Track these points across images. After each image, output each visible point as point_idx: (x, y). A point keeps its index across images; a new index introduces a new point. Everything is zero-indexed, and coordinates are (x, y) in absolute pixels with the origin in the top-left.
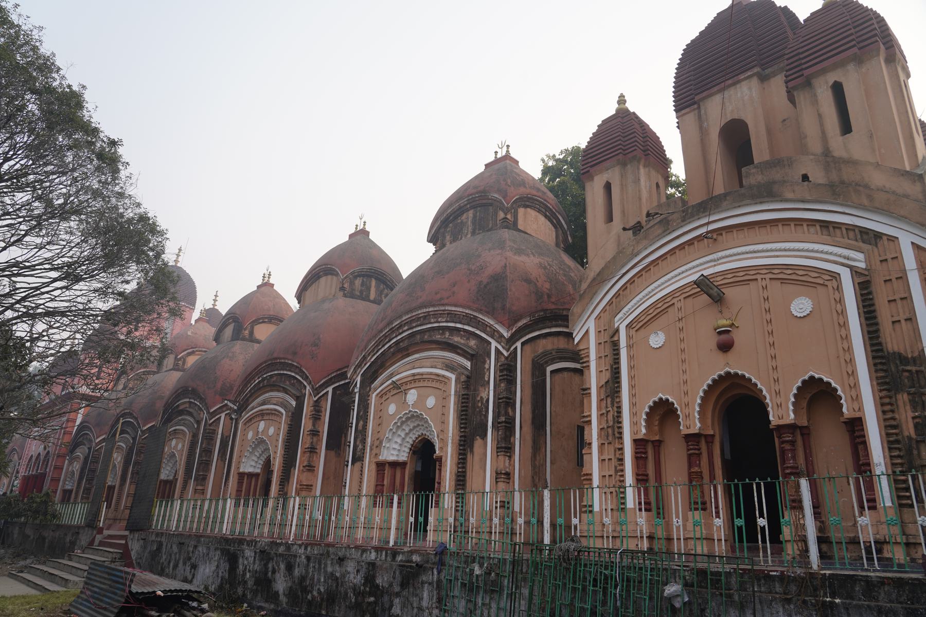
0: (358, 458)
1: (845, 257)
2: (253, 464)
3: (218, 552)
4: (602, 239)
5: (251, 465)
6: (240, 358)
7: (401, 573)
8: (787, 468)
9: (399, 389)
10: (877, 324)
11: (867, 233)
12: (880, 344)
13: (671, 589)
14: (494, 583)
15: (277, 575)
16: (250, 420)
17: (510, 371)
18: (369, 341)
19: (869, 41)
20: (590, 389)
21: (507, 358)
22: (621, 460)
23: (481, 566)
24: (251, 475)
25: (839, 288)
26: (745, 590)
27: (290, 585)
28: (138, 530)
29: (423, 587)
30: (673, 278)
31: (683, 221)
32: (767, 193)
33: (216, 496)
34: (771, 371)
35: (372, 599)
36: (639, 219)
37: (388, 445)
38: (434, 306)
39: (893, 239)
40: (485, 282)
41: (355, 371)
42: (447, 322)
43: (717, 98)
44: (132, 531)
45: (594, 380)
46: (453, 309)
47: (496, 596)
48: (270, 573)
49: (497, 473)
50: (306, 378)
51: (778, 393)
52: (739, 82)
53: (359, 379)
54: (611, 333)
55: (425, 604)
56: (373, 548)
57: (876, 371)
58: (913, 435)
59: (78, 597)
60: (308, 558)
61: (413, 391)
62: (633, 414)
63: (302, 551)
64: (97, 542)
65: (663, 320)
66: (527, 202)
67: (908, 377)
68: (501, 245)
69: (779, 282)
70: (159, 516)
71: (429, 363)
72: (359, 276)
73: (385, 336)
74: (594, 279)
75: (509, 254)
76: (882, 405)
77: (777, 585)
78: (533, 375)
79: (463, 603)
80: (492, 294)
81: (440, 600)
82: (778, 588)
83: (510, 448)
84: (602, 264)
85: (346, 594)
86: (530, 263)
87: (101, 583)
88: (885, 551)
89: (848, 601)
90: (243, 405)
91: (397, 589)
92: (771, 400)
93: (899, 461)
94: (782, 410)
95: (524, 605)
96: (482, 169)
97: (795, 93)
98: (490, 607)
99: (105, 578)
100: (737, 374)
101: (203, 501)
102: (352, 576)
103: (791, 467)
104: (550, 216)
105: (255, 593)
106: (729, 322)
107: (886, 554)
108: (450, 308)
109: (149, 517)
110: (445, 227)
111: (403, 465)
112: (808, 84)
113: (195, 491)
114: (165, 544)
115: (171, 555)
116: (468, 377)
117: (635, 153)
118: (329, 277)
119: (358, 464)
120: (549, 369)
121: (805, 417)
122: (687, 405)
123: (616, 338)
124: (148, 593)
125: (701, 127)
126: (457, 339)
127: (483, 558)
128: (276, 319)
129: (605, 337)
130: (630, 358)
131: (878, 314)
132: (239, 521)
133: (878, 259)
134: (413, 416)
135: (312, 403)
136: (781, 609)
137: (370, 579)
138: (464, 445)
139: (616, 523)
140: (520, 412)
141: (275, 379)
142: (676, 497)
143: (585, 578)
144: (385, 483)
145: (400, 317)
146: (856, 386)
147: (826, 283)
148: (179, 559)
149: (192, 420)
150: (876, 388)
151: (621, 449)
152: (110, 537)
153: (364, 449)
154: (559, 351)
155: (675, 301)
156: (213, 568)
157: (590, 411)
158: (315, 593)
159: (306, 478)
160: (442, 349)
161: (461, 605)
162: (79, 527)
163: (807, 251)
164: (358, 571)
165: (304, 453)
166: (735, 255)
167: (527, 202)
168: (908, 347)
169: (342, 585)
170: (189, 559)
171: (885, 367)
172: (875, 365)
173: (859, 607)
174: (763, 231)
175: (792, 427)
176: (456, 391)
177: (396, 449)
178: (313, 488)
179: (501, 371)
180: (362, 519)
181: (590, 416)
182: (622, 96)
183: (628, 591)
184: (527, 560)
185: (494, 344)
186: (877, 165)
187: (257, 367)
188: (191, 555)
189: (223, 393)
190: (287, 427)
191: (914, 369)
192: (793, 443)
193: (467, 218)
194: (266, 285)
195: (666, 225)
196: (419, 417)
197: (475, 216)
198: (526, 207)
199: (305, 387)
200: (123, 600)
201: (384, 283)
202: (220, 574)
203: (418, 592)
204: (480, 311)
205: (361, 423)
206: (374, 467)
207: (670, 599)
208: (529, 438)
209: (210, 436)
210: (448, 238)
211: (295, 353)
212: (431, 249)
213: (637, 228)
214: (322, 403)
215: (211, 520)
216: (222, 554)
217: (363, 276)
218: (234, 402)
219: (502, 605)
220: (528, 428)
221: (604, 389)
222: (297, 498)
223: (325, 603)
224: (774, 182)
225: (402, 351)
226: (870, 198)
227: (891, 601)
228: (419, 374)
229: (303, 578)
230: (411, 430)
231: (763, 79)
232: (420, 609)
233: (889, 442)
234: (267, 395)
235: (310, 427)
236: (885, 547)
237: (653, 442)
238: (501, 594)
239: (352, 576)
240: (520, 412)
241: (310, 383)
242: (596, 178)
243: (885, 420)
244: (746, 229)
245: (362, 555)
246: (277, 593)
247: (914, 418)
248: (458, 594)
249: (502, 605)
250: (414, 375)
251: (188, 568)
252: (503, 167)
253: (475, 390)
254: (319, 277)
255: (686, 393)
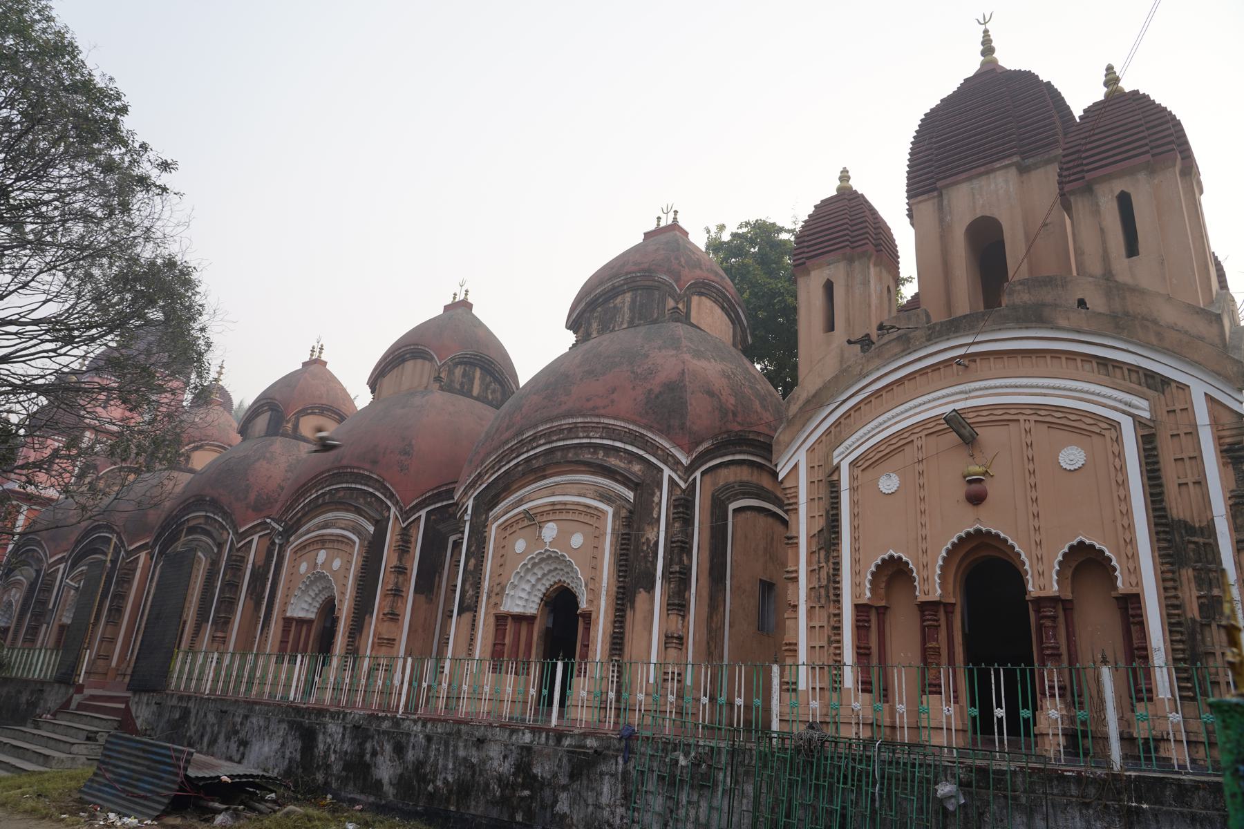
0: (469, 607)
1: (1126, 404)
2: (306, 606)
3: (284, 726)
4: (817, 354)
5: (303, 608)
6: (284, 461)
7: (570, 761)
8: (1048, 648)
9: (533, 520)
10: (1161, 485)
11: (1153, 377)
12: (1164, 509)
13: (945, 789)
14: (705, 776)
15: (380, 759)
16: (303, 547)
17: (687, 508)
18: (489, 454)
19: (1165, 148)
20: (797, 537)
21: (683, 491)
22: (838, 629)
23: (686, 755)
24: (301, 622)
25: (1118, 440)
26: (1034, 792)
27: (399, 771)
28: (153, 691)
29: (602, 779)
30: (911, 409)
31: (928, 340)
32: (1035, 316)
33: (245, 647)
34: (1032, 532)
35: (527, 793)
36: (867, 331)
37: (512, 593)
38: (584, 416)
39: (1183, 387)
40: (657, 390)
41: (465, 493)
42: (601, 438)
43: (964, 189)
44: (135, 692)
45: (803, 525)
46: (612, 422)
47: (707, 793)
48: (368, 756)
49: (667, 637)
50: (391, 496)
51: (1040, 559)
52: (993, 170)
53: (470, 503)
54: (828, 471)
55: (604, 800)
56: (527, 728)
57: (1158, 540)
58: (1198, 618)
59: (91, 780)
60: (429, 739)
61: (550, 524)
62: (856, 573)
63: (418, 728)
64: (74, 705)
65: (898, 460)
66: (703, 288)
67: (1194, 550)
68: (675, 344)
69: (1046, 426)
70: (181, 672)
71: (574, 490)
72: (461, 363)
73: (511, 450)
74: (808, 402)
75: (687, 357)
76: (1164, 580)
77: (1073, 787)
78: (712, 514)
79: (660, 800)
80: (666, 408)
81: (627, 796)
82: (1074, 790)
83: (684, 606)
84: (818, 384)
85: (487, 785)
86: (711, 369)
87: (130, 762)
88: (1161, 750)
89: (1157, 807)
90: (292, 526)
91: (564, 781)
92: (1031, 566)
93: (1181, 646)
94: (1044, 579)
95: (747, 804)
96: (639, 239)
97: (1072, 199)
98: (699, 807)
99: (138, 757)
100: (989, 533)
101: (222, 654)
102: (496, 763)
103: (1052, 648)
104: (728, 308)
105: (344, 781)
106: (982, 469)
107: (1162, 754)
108: (607, 421)
109: (166, 673)
110: (593, 310)
111: (530, 619)
112: (1088, 189)
113: (213, 639)
114: (194, 712)
115: (204, 727)
116: (630, 512)
117: (865, 248)
118: (419, 361)
119: (467, 616)
120: (732, 506)
121: (1069, 589)
122: (926, 566)
123: (835, 477)
124: (211, 778)
125: (941, 221)
126: (613, 462)
127: (689, 745)
128: (328, 410)
129: (819, 475)
130: (854, 503)
131: (1163, 473)
132: (195, 677)
133: (1165, 409)
134: (549, 557)
135: (398, 530)
136: (1078, 815)
137: (523, 768)
138: (622, 599)
139: (826, 706)
140: (697, 561)
141: (342, 494)
142: (902, 681)
143: (832, 775)
144: (507, 641)
145: (535, 426)
146: (1134, 556)
147: (1104, 432)
148: (219, 733)
149: (210, 541)
150: (1158, 560)
151: (839, 615)
152: (93, 698)
153: (477, 596)
154: (743, 484)
155: (914, 437)
156: (276, 746)
157: (797, 564)
158: (439, 783)
159: (387, 630)
160: (593, 473)
161: (658, 803)
162: (43, 683)
163: (1081, 391)
164: (505, 757)
165: (385, 596)
166: (991, 388)
167: (703, 288)
168: (1195, 515)
169: (481, 774)
170: (236, 732)
171: (1169, 537)
172: (1157, 533)
173: (1171, 813)
174: (1026, 361)
175: (1054, 600)
176: (613, 529)
177: (523, 599)
178: (396, 643)
179: (675, 507)
180: (332, 679)
181: (796, 571)
182: (845, 171)
183: (889, 790)
184: (751, 750)
185: (667, 472)
186: (1169, 298)
187: (316, 476)
188: (238, 727)
189: (260, 506)
190: (360, 559)
191: (1201, 540)
192: (1054, 618)
193: (623, 303)
194: (315, 364)
195: (906, 343)
196: (559, 559)
197: (633, 301)
198: (701, 294)
199: (389, 509)
200: (176, 787)
201: (492, 375)
202: (288, 755)
203: (595, 785)
204: (650, 428)
205: (472, 562)
206: (492, 620)
207: (941, 801)
208: (705, 593)
209: (236, 565)
210: (595, 325)
211: (375, 462)
212: (571, 338)
213: (866, 342)
214: (412, 531)
215: (233, 679)
216: (291, 728)
217: (465, 363)
218: (278, 521)
219: (715, 803)
220: (705, 581)
221: (816, 539)
222: (410, 660)
223: (454, 798)
224: (1044, 305)
225: (535, 471)
226: (1159, 335)
227: (1206, 808)
228: (560, 503)
229: (420, 764)
230: (544, 575)
231: (1023, 170)
232: (598, 806)
233: (1170, 624)
234: (330, 515)
235: (394, 561)
236: (1162, 745)
237: (877, 608)
238: (714, 791)
239: (496, 763)
240: (697, 561)
241: (396, 503)
242: (813, 273)
243: (1166, 598)
244: (1005, 358)
245: (510, 736)
246: (379, 783)
247: (1198, 598)
248: (652, 789)
249: (715, 803)
250: (553, 504)
251: (233, 746)
252: (667, 237)
253: (639, 529)
254: (404, 361)
255: (925, 552)
